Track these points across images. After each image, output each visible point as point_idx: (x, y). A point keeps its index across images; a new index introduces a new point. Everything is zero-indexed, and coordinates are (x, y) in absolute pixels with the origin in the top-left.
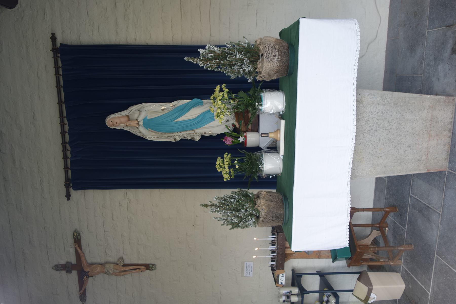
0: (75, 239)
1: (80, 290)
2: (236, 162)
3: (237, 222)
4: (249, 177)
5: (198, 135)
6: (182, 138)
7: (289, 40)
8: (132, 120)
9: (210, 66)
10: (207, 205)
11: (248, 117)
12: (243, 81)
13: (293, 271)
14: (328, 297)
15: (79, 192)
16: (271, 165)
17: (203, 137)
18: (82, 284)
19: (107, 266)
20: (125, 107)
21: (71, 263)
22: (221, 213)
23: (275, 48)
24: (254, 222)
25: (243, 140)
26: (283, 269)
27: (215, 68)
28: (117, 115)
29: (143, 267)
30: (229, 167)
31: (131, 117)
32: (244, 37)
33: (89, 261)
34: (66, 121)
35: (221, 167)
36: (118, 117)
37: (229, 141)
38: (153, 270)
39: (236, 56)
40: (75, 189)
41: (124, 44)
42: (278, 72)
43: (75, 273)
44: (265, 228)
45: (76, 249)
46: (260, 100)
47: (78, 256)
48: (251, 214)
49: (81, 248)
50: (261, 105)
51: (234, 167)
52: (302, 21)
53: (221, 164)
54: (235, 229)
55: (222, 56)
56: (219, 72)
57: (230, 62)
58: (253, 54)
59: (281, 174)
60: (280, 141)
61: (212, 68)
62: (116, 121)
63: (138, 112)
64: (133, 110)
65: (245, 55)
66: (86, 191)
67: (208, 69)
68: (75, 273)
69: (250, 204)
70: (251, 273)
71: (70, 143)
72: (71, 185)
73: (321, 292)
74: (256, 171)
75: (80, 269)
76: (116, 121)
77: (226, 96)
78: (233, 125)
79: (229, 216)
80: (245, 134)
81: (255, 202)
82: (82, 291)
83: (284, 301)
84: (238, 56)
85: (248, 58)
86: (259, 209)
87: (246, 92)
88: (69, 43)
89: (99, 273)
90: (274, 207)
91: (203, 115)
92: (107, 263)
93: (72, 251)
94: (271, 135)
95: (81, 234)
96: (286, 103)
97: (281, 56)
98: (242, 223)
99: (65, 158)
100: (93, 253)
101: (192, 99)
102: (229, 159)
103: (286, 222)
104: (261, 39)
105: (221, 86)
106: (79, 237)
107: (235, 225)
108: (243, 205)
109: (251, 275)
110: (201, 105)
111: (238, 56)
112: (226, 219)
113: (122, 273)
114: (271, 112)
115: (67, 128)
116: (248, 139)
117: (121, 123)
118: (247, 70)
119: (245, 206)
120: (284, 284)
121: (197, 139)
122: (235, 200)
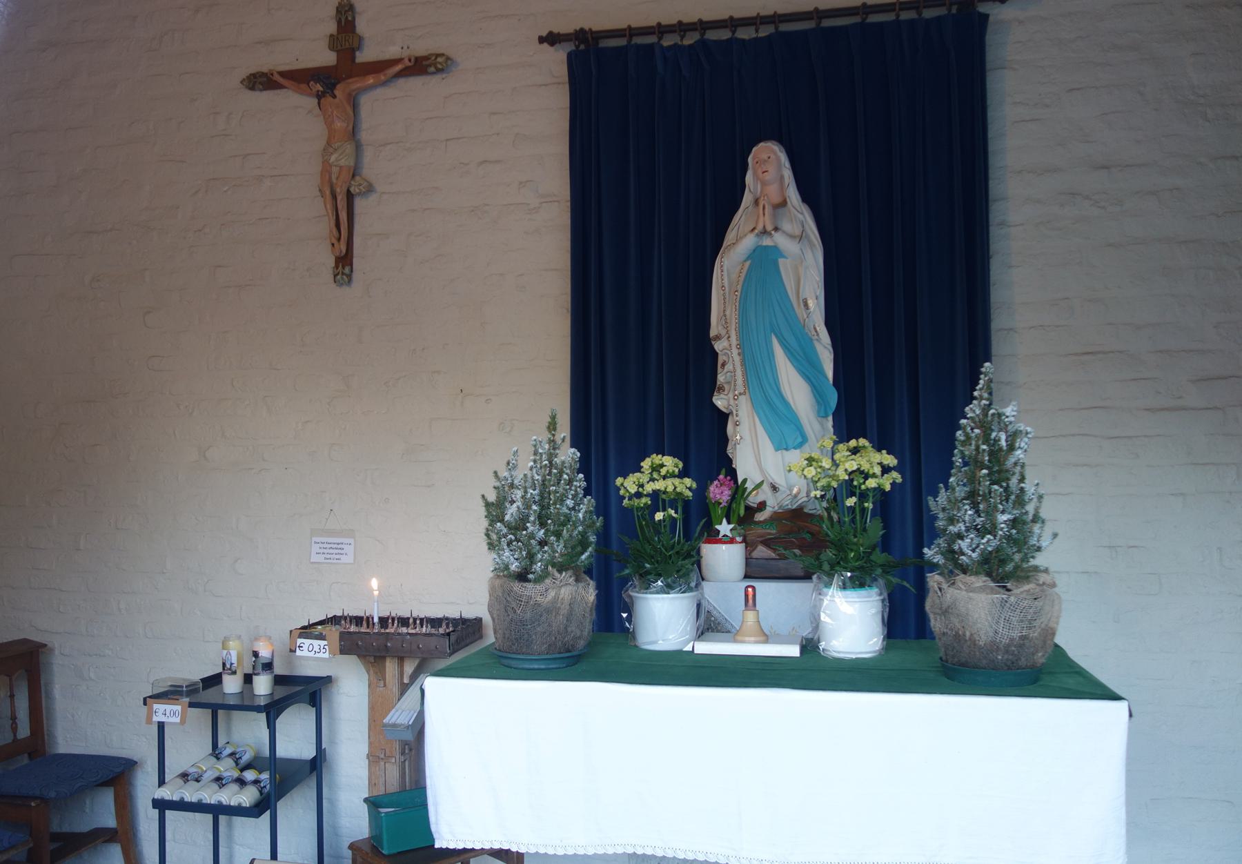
0: (427, 58)
1: (282, 74)
2: (672, 512)
3: (507, 518)
4: (630, 553)
5: (732, 402)
6: (721, 359)
7: (1039, 671)
8: (775, 217)
9: (968, 438)
10: (555, 429)
11: (800, 545)
12: (924, 530)
13: (327, 680)
14: (256, 782)
15: (562, 71)
16: (663, 618)
17: (723, 417)
18: (299, 78)
19: (349, 148)
20: (807, 196)
21: (359, 48)
22: (531, 469)
23: (1030, 628)
24: (507, 567)
25: (721, 534)
26: (342, 652)
27: (962, 452)
28: (788, 174)
29: (343, 247)
30: (655, 495)
31: (781, 211)
32: (1055, 535)
33: (365, 101)
34: (765, 31)
35: (656, 468)
36: (782, 178)
37: (718, 492)
38: (335, 276)
39: (1003, 512)
40: (570, 56)
41: (990, 193)
42: (958, 637)
43: (328, 58)
44: (484, 598)
45: (399, 61)
46: (858, 582)
47: (378, 67)
48: (531, 557)
49: (399, 75)
50: (844, 587)
51: (654, 508)
52: (1121, 708)
53: (663, 471)
54: (482, 511)
55: (999, 472)
56: (951, 465)
57: (984, 496)
58: (1006, 566)
59: (636, 646)
60: (735, 641)
61: (964, 443)
62: (769, 168)
63: (797, 232)
64: (801, 217)
65: (1009, 538)
66: (567, 87)
67: (959, 433)
68: (328, 58)
69: (562, 555)
70: (320, 558)
71: (703, 43)
72: (582, 47)
73: (271, 762)
74: (648, 573)
75: (340, 76)
76: (769, 168)
77: (871, 483)
78: (762, 506)
79: (526, 492)
80: (739, 539)
81: (566, 570)
82: (277, 78)
83: (256, 654)
84: (1005, 517)
85: (998, 550)
86: (548, 581)
87: (886, 543)
88: (990, 38)
89: (329, 124)
90: (550, 625)
91: (792, 419)
92: (358, 148)
93: (392, 52)
94: (750, 615)
95: (438, 77)
96: (852, 660)
97: (1009, 645)
98: (505, 530)
99: (661, 30)
100: (385, 109)
101: (835, 384)
102: (681, 494)
103: (505, 662)
104: (1054, 585)
105: (894, 469)
106: (432, 69)
107: (495, 511)
108: (558, 535)
109: (315, 558)
110: (819, 412)
111: (1005, 517)
112: (512, 486)
113: (328, 193)
114: (823, 617)
115: (745, 34)
116: (724, 547)
117: (764, 184)
118: (964, 544)
119: (558, 541)
120: (298, 653)
121: (720, 402)
122: (569, 509)
